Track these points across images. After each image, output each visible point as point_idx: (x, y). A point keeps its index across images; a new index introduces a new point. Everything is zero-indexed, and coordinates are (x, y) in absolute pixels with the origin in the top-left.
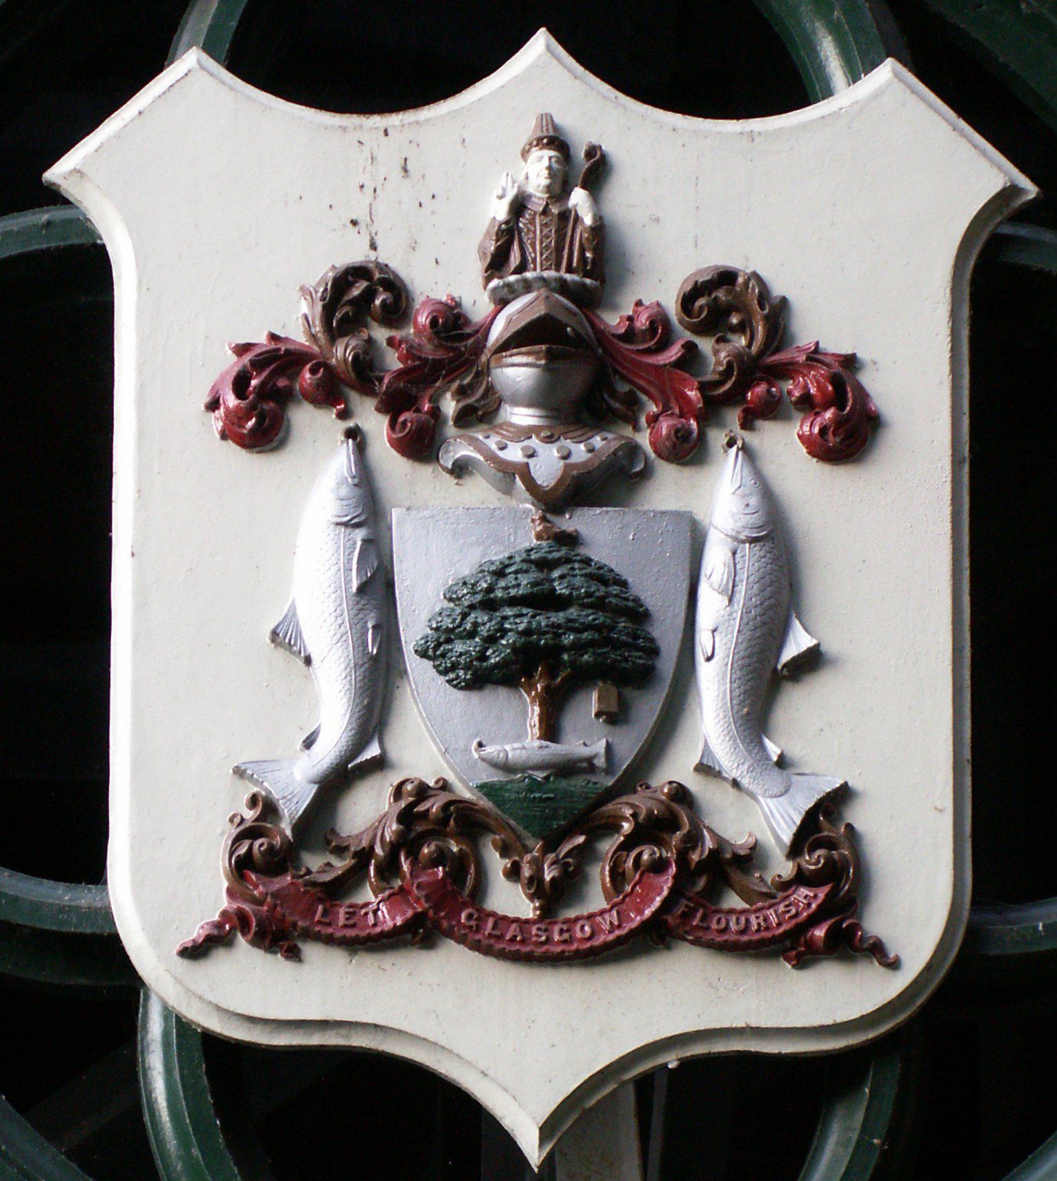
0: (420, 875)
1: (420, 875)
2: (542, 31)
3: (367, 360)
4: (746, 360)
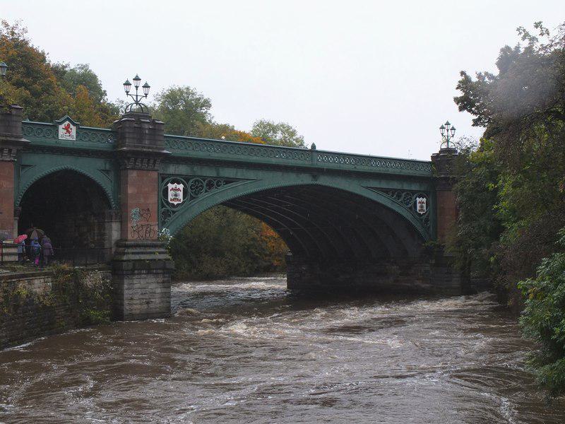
0: (173, 200)
4: (179, 190)
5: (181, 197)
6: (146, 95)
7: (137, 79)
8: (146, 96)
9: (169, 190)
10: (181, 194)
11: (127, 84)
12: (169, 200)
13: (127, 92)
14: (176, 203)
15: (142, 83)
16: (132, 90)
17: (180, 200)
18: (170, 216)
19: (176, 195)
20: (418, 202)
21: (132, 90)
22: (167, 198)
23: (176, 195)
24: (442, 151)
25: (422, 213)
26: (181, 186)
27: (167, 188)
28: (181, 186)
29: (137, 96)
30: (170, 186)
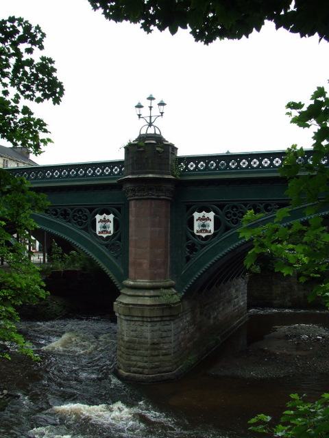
0: (201, 231)
1: (201, 231)
2: (266, 21)
3: (199, 219)
4: (208, 219)
5: (111, 228)
6: (162, 113)
7: (151, 98)
8: (162, 115)
9: (97, 222)
10: (111, 225)
11: (139, 106)
12: (195, 232)
13: (139, 115)
14: (105, 236)
15: (146, 103)
16: (145, 112)
17: (110, 233)
18: (196, 251)
19: (204, 226)
20: (98, 220)
21: (145, 112)
22: (193, 230)
23: (204, 226)
24: (142, 138)
25: (105, 236)
26: (211, 215)
27: (193, 217)
28: (211, 215)
29: (151, 117)
30: (98, 217)
